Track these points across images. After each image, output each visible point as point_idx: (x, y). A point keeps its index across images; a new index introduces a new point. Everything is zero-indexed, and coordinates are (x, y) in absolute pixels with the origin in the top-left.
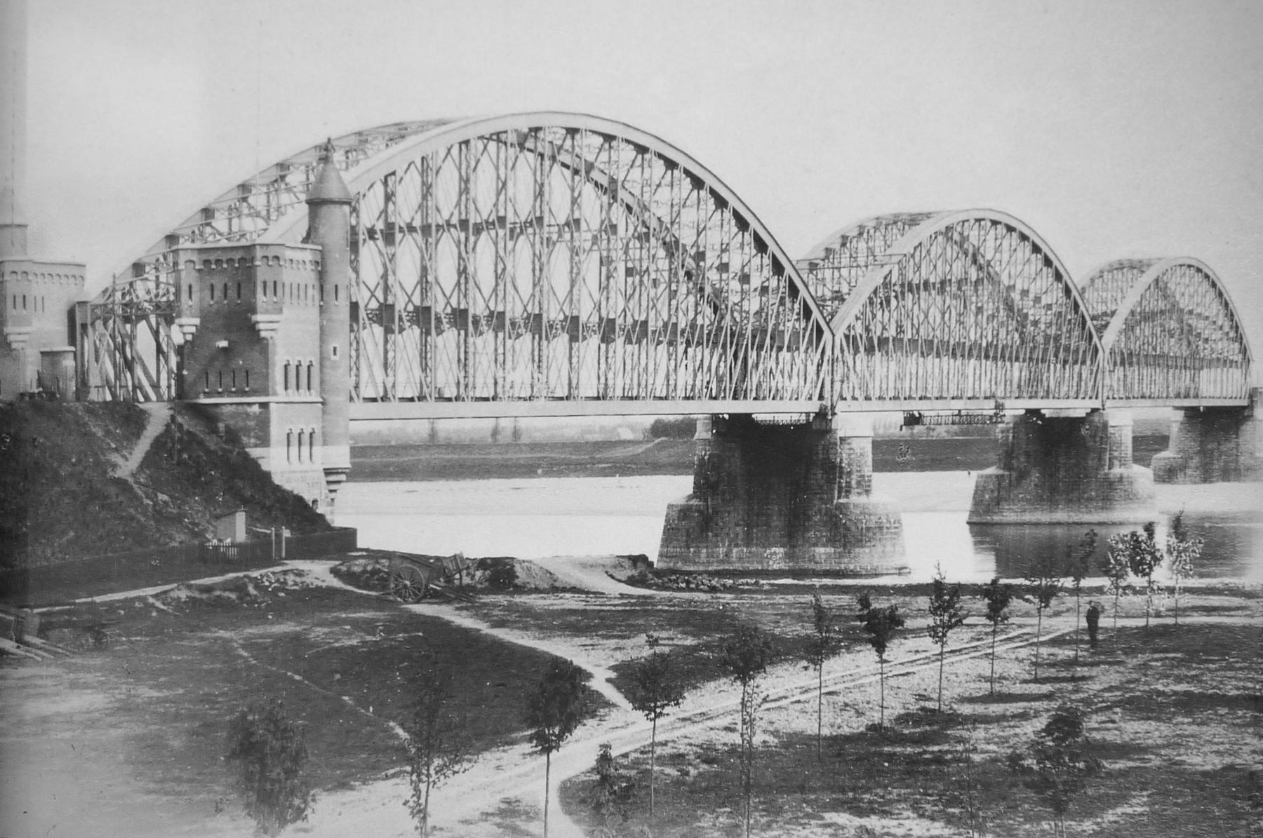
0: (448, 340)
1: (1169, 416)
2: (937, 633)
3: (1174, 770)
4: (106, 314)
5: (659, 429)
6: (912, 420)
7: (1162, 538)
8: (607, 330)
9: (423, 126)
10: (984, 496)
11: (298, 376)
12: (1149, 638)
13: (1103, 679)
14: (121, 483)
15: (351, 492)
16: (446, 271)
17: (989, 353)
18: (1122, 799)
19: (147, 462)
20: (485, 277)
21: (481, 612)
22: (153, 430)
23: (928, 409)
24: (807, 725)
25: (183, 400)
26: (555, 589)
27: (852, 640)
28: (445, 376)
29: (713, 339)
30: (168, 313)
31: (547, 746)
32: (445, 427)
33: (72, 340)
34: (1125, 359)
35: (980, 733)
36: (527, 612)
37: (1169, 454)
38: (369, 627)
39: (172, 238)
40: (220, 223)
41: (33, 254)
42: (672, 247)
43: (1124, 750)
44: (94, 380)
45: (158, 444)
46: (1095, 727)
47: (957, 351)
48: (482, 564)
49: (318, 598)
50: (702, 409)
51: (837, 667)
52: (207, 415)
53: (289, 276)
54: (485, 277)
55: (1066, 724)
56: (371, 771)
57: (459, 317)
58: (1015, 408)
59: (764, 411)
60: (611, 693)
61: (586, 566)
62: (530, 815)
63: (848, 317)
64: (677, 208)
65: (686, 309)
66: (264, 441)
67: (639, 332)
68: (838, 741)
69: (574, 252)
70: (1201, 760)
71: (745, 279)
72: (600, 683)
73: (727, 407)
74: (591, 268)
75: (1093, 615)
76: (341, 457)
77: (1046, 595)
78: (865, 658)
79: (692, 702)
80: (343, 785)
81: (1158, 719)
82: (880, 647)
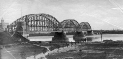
0: (36, 28)
1: (86, 31)
2: (71, 45)
3: (88, 53)
4: (10, 26)
5: (51, 33)
6: (69, 32)
7: (86, 39)
8: (47, 27)
9: (33, 14)
10: (12, 29)
11: (25, 30)
12: (86, 45)
13: (83, 48)
14: (12, 37)
15: (29, 37)
16: (36, 23)
17: (74, 28)
18: (85, 55)
19: (13, 36)
20: (44, 24)
21: (39, 45)
22: (14, 34)
23: (70, 31)
24: (63, 51)
25: (16, 31)
26: (44, 43)
27: (65, 46)
28: (36, 30)
29: (55, 27)
30: (15, 26)
31: (44, 53)
32: (36, 33)
33: (8, 28)
34: (83, 28)
35: (75, 51)
36: (42, 45)
37: (86, 34)
38: (31, 46)
39: (15, 21)
40: (19, 20)
41: (5, 22)
42: (52, 22)
43: (84, 52)
44: (9, 30)
45: (14, 35)
46: (82, 51)
47: (72, 28)
48: (39, 42)
49: (26, 44)
50: (54, 32)
51: (65, 48)
52: (18, 33)
53: (24, 24)
54: (44, 24)
55: (80, 50)
56: (31, 55)
57: (37, 26)
58: (76, 31)
59: (59, 32)
60: (49, 50)
61: (46, 41)
62: (43, 58)
63: (64, 26)
64: (52, 19)
65: (75, 27)
66: (22, 34)
67: (49, 27)
68: (65, 52)
69: (45, 22)
70: (90, 52)
71: (57, 23)
72: (48, 49)
73: (56, 31)
74: (46, 23)
75: (82, 44)
76: (28, 35)
77: (79, 43)
78: (67, 47)
79: (55, 50)
80: (29, 56)
81: (119, 54)
82: (68, 46)
